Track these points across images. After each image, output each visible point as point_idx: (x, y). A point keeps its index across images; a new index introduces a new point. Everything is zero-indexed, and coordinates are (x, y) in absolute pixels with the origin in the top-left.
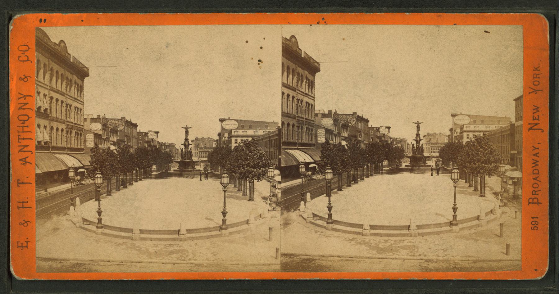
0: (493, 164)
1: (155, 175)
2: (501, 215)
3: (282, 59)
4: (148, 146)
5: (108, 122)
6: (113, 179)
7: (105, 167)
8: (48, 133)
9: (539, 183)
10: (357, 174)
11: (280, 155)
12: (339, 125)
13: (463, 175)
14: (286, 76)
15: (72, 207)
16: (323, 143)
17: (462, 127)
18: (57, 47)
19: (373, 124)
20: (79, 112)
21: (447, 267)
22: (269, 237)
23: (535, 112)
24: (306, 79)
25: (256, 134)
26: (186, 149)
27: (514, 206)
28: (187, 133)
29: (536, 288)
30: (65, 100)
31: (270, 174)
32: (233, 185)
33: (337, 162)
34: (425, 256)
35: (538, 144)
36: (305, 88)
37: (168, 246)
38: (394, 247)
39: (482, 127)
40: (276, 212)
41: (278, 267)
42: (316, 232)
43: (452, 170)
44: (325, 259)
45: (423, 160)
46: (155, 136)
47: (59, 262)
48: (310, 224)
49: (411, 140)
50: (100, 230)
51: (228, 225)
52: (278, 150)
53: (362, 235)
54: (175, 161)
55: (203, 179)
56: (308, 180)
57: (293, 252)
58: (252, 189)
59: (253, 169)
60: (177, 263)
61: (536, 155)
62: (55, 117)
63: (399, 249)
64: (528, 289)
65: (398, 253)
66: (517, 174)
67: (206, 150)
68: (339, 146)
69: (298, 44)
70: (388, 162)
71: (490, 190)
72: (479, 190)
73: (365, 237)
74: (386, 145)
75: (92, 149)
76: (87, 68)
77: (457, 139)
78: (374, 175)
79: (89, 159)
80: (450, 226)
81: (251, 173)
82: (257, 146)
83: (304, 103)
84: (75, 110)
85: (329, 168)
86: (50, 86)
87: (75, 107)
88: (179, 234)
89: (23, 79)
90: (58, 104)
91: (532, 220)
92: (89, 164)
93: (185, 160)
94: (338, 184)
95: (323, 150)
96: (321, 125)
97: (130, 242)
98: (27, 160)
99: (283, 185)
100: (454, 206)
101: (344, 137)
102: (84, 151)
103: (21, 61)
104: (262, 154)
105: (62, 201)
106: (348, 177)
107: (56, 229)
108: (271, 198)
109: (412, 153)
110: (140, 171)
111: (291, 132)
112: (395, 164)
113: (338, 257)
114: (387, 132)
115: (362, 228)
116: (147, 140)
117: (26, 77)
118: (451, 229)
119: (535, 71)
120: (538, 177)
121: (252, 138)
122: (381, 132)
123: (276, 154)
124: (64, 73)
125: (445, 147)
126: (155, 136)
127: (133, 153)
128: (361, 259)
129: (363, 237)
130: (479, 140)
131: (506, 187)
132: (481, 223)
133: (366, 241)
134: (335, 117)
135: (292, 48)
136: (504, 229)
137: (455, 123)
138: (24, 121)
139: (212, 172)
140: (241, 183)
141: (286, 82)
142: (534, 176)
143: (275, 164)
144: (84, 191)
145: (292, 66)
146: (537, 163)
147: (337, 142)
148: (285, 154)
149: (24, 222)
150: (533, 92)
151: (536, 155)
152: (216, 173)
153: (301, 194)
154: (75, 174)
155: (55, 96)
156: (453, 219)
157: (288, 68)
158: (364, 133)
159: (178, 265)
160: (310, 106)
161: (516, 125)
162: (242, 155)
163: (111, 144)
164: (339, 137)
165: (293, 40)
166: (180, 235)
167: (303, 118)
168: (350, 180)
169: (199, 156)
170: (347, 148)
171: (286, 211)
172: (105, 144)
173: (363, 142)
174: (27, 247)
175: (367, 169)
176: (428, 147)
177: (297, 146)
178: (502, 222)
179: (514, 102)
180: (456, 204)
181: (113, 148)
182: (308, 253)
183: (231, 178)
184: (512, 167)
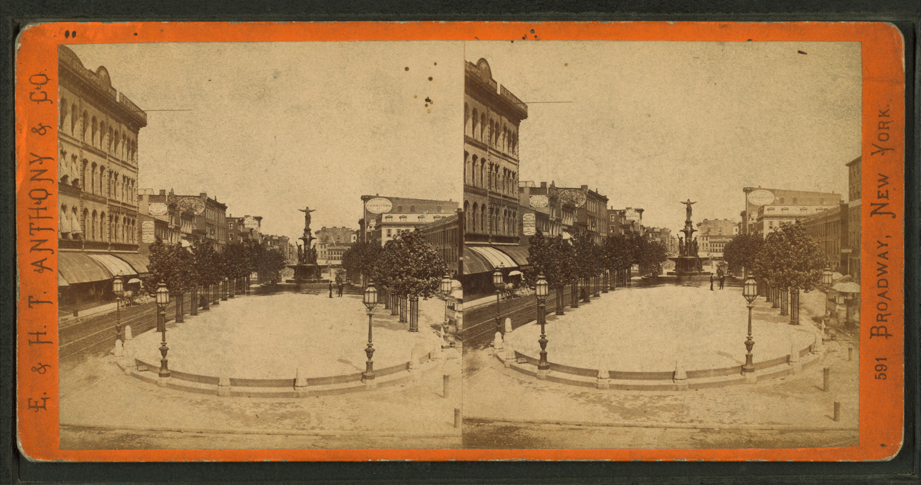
1: (255, 288)
2: (825, 354)
4: (244, 240)
5: (177, 201)
6: (186, 296)
7: (173, 275)
9: (888, 302)
10: (589, 287)
11: (462, 256)
12: (559, 206)
13: (762, 289)
14: (471, 126)
15: (118, 342)
16: (532, 237)
17: (761, 210)
18: (94, 78)
20: (130, 185)
23: (882, 185)
25: (421, 221)
26: (688, 238)
28: (308, 219)
29: (883, 475)
30: (108, 165)
31: (446, 287)
33: (554, 267)
34: (701, 422)
35: (887, 237)
36: (502, 145)
37: (277, 405)
38: (649, 407)
39: (794, 210)
40: (455, 349)
41: (458, 441)
42: (521, 383)
43: (745, 280)
44: (536, 428)
46: (637, 216)
47: (98, 432)
48: (510, 370)
49: (676, 231)
50: (165, 380)
51: (376, 371)
52: (458, 248)
53: (597, 388)
55: (334, 295)
56: (508, 297)
57: (483, 416)
58: (415, 312)
59: (417, 278)
60: (670, 428)
61: (883, 255)
62: (91, 193)
63: (657, 410)
64: (870, 477)
65: (656, 418)
66: (852, 288)
67: (339, 247)
68: (559, 242)
69: (490, 73)
71: (807, 313)
72: (789, 313)
74: (636, 239)
75: (151, 246)
76: (143, 112)
79: (147, 262)
80: (741, 373)
81: (413, 286)
83: (501, 170)
84: (124, 181)
85: (541, 277)
86: (82, 143)
87: (124, 177)
90: (95, 171)
91: (877, 363)
92: (147, 271)
95: (532, 247)
96: (528, 206)
98: (45, 264)
99: (467, 305)
101: (566, 226)
102: (138, 249)
103: (35, 100)
104: (431, 254)
106: (574, 292)
107: (92, 378)
108: (446, 326)
109: (678, 252)
110: (230, 282)
112: (651, 271)
113: (558, 423)
114: (638, 218)
115: (596, 376)
117: (43, 127)
118: (744, 377)
119: (881, 118)
121: (415, 227)
122: (627, 219)
124: (105, 121)
125: (733, 242)
126: (255, 224)
128: (594, 428)
129: (599, 391)
130: (790, 232)
132: (793, 369)
134: (552, 193)
136: (831, 377)
138: (40, 199)
139: (349, 284)
141: (471, 135)
142: (881, 291)
143: (453, 271)
144: (138, 315)
145: (482, 108)
146: (885, 269)
147: (556, 234)
148: (469, 255)
149: (40, 366)
150: (879, 151)
151: (883, 255)
152: (356, 285)
153: (496, 319)
154: (124, 287)
155: (91, 158)
156: (747, 361)
157: (475, 112)
158: (600, 220)
159: (293, 437)
160: (511, 175)
161: (850, 206)
162: (398, 256)
163: (183, 238)
164: (177, 234)
165: (483, 66)
167: (499, 195)
168: (577, 298)
169: (709, 250)
170: (571, 244)
171: (471, 348)
172: (173, 238)
173: (598, 234)
174: (44, 407)
175: (605, 278)
176: (705, 242)
177: (490, 240)
178: (827, 367)
179: (847, 168)
180: (752, 336)
181: (185, 244)
182: (507, 418)
183: (381, 293)
184: (843, 275)
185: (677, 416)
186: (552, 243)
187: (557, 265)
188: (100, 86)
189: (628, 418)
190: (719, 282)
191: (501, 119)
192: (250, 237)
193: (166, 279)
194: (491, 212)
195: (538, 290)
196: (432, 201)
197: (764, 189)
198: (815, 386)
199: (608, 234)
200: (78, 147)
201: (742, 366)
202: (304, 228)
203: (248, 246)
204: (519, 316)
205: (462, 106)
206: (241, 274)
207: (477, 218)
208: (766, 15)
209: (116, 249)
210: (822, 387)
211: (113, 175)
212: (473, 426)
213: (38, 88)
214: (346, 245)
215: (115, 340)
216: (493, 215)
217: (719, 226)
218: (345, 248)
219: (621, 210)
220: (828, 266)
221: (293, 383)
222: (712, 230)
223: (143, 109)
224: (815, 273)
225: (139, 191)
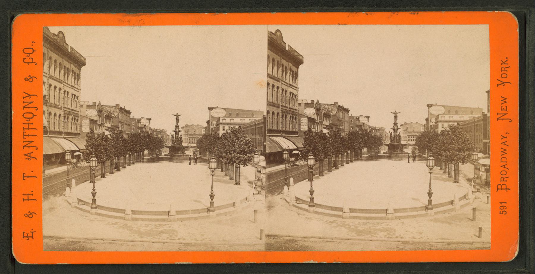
0: (247, 155)
3: (268, 52)
4: (140, 132)
7: (318, 149)
8: (47, 118)
10: (338, 161)
11: (265, 142)
12: (103, 116)
14: (271, 68)
16: (306, 132)
18: (56, 37)
19: (135, 115)
22: (254, 219)
24: (72, 73)
26: (177, 135)
29: (508, 270)
32: (220, 170)
34: (402, 238)
35: (506, 133)
36: (289, 79)
37: (158, 226)
39: (456, 118)
41: (263, 248)
43: (428, 157)
46: (147, 122)
48: (75, 209)
49: (388, 129)
50: (94, 211)
52: (263, 137)
53: (124, 220)
56: (292, 166)
58: (238, 173)
60: (384, 241)
61: (504, 143)
62: (53, 103)
63: (377, 231)
64: (501, 271)
66: (487, 162)
67: (195, 136)
68: (321, 134)
69: (282, 38)
71: (463, 176)
72: (453, 176)
73: (345, 220)
75: (305, 132)
76: (84, 57)
77: (432, 128)
78: (135, 163)
79: (85, 143)
80: (425, 210)
81: (456, 156)
83: (288, 94)
84: (290, 95)
85: (94, 156)
86: (48, 74)
88: (386, 213)
89: (28, 216)
90: (56, 91)
92: (85, 148)
93: (394, 143)
96: (85, 116)
98: (32, 155)
99: (268, 170)
101: (325, 125)
102: (80, 136)
104: (248, 141)
106: (330, 162)
108: (256, 182)
110: (132, 155)
111: (276, 121)
113: (320, 238)
116: (139, 126)
117: (31, 214)
122: (360, 122)
123: (261, 141)
124: (279, 61)
126: (147, 122)
127: (126, 138)
128: (341, 241)
129: (343, 220)
132: (455, 208)
133: (346, 224)
136: (477, 213)
137: (430, 113)
139: (419, 155)
140: (447, 165)
141: (271, 73)
142: (503, 164)
143: (260, 151)
144: (79, 173)
145: (277, 58)
146: (505, 152)
147: (319, 130)
148: (269, 141)
149: (30, 77)
154: (71, 157)
155: (54, 83)
157: (273, 60)
158: (345, 122)
163: (324, 128)
164: (321, 126)
165: (278, 34)
166: (169, 216)
168: (331, 166)
169: (188, 142)
171: (270, 195)
173: (343, 130)
174: (32, 237)
176: (405, 135)
178: (474, 207)
179: (487, 93)
180: (213, 191)
181: (325, 131)
182: (291, 234)
183: (218, 162)
184: (484, 155)
187: (320, 147)
188: (59, 42)
189: (360, 236)
190: (413, 158)
191: (288, 64)
194: (64, 119)
195: (309, 162)
197: (439, 105)
200: (46, 77)
202: (394, 123)
203: (143, 135)
204: (80, 178)
205: (266, 57)
207: (274, 120)
208: (441, 8)
209: (285, 134)
211: (66, 93)
212: (53, 241)
213: (28, 56)
214: (418, 132)
215: (66, 187)
223: (83, 56)
225: (81, 102)
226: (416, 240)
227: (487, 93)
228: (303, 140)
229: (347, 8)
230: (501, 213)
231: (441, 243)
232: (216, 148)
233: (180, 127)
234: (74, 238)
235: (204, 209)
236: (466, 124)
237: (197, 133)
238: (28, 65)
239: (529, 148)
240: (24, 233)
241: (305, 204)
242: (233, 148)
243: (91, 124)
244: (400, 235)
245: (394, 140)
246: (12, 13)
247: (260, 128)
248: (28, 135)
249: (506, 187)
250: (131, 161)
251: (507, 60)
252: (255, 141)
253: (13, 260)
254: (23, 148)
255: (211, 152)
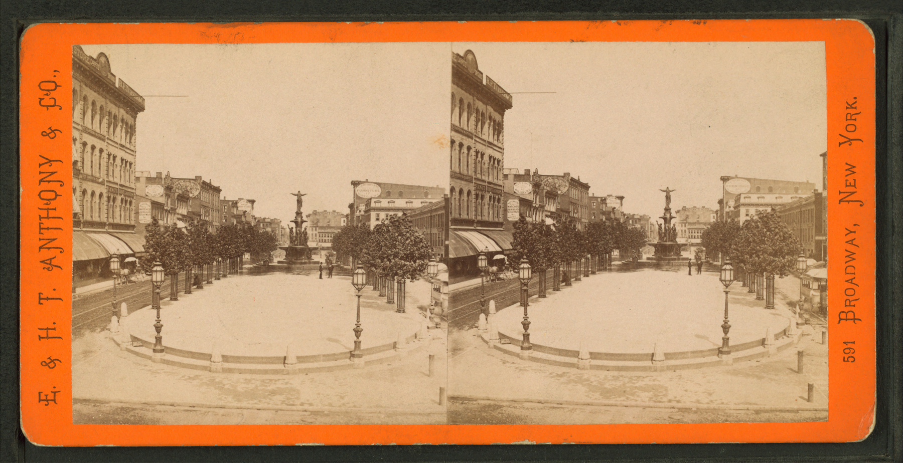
0: (418, 261)
1: (248, 269)
3: (452, 88)
4: (237, 222)
5: (542, 181)
6: (549, 272)
8: (79, 199)
11: (448, 240)
12: (174, 196)
14: (458, 115)
15: (114, 319)
16: (516, 222)
17: (738, 197)
18: (94, 63)
19: (227, 194)
21: (713, 421)
22: (429, 371)
26: (298, 229)
27: (821, 324)
32: (372, 287)
33: (537, 251)
34: (678, 402)
35: (855, 225)
36: (487, 133)
37: (636, 378)
39: (770, 199)
40: (810, 326)
41: (443, 419)
43: (722, 266)
45: (306, 253)
46: (248, 207)
47: (93, 404)
48: (126, 353)
49: (656, 217)
52: (444, 232)
54: (648, 244)
55: (324, 276)
56: (492, 280)
57: (467, 395)
58: (402, 292)
59: (405, 261)
60: (649, 407)
61: (851, 242)
62: (458, 172)
63: (636, 390)
66: (823, 273)
67: (329, 230)
68: (542, 227)
70: (251, 255)
71: (782, 297)
72: (765, 297)
73: (583, 372)
74: (248, 228)
75: (515, 224)
77: (730, 217)
79: (144, 242)
80: (718, 355)
81: (769, 264)
82: (411, 224)
83: (486, 158)
86: (81, 126)
89: (47, 364)
93: (666, 241)
94: (540, 288)
96: (144, 195)
97: (205, 374)
98: (54, 262)
99: (453, 287)
100: (357, 326)
101: (549, 212)
104: (418, 238)
105: (99, 308)
106: (188, 279)
108: (432, 308)
110: (223, 263)
111: (466, 204)
113: (540, 402)
118: (352, 363)
120: (854, 278)
122: (608, 205)
123: (440, 239)
124: (472, 103)
126: (248, 207)
128: (576, 407)
131: (806, 292)
135: (468, 70)
136: (805, 360)
137: (726, 191)
139: (708, 262)
141: (457, 124)
142: (850, 277)
143: (439, 255)
144: (133, 292)
145: (468, 98)
146: (853, 256)
147: (539, 220)
148: (455, 239)
150: (847, 141)
153: (481, 301)
154: (120, 265)
155: (91, 140)
156: (723, 344)
157: (461, 101)
158: (581, 206)
163: (547, 216)
165: (470, 57)
166: (286, 365)
167: (117, 184)
168: (559, 281)
172: (169, 219)
173: (211, 224)
174: (54, 400)
176: (684, 228)
178: (801, 350)
179: (822, 158)
180: (728, 319)
181: (549, 221)
182: (491, 396)
183: (369, 274)
184: (817, 262)
185: (656, 396)
186: (535, 228)
187: (540, 249)
188: (100, 72)
190: (697, 267)
191: (487, 109)
192: (612, 215)
193: (162, 259)
194: (477, 198)
195: (521, 273)
196: (419, 186)
198: (421, 372)
199: (590, 219)
201: (719, 348)
202: (296, 211)
206: (602, 251)
208: (744, 14)
209: (481, 227)
210: (797, 370)
213: (47, 95)
214: (705, 224)
216: (478, 201)
217: (697, 213)
218: (335, 231)
219: (602, 197)
220: (802, 252)
221: (651, 358)
222: (321, 221)
223: (141, 95)
224: (789, 259)
225: (136, 173)
226: (702, 405)
227: (822, 158)
228: (511, 236)
229: (585, 13)
230: (846, 359)
231: (744, 412)
232: (364, 251)
233: (304, 215)
234: (125, 403)
235: (345, 353)
236: (786, 209)
237: (332, 224)
238: (48, 109)
239: (893, 249)
240: (41, 394)
241: (515, 344)
242: (394, 250)
243: (154, 210)
244: (675, 397)
245: (665, 236)
246: (20, 22)
247: (440, 216)
248: (48, 229)
249: (854, 316)
250: (221, 272)
251: (856, 102)
252: (431, 238)
253: (22, 439)
254: (40, 251)
255: (356, 257)
